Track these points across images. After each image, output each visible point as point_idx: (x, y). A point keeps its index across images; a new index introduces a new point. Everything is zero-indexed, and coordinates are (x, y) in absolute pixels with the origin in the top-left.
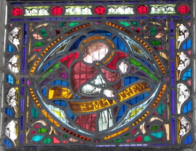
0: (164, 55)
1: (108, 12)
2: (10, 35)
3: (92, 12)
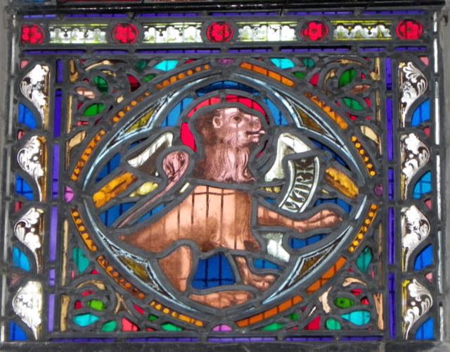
0: (370, 133)
1: (239, 37)
3: (203, 38)
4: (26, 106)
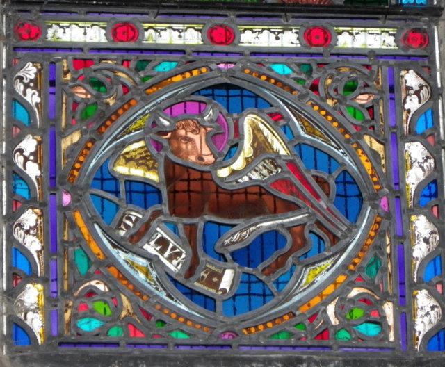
2: (18, 228)
4: (17, 249)
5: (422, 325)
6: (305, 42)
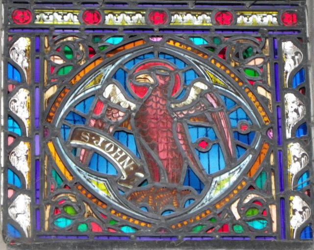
5: (296, 222)
6: (215, 22)
